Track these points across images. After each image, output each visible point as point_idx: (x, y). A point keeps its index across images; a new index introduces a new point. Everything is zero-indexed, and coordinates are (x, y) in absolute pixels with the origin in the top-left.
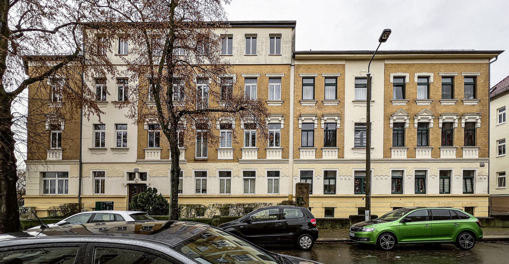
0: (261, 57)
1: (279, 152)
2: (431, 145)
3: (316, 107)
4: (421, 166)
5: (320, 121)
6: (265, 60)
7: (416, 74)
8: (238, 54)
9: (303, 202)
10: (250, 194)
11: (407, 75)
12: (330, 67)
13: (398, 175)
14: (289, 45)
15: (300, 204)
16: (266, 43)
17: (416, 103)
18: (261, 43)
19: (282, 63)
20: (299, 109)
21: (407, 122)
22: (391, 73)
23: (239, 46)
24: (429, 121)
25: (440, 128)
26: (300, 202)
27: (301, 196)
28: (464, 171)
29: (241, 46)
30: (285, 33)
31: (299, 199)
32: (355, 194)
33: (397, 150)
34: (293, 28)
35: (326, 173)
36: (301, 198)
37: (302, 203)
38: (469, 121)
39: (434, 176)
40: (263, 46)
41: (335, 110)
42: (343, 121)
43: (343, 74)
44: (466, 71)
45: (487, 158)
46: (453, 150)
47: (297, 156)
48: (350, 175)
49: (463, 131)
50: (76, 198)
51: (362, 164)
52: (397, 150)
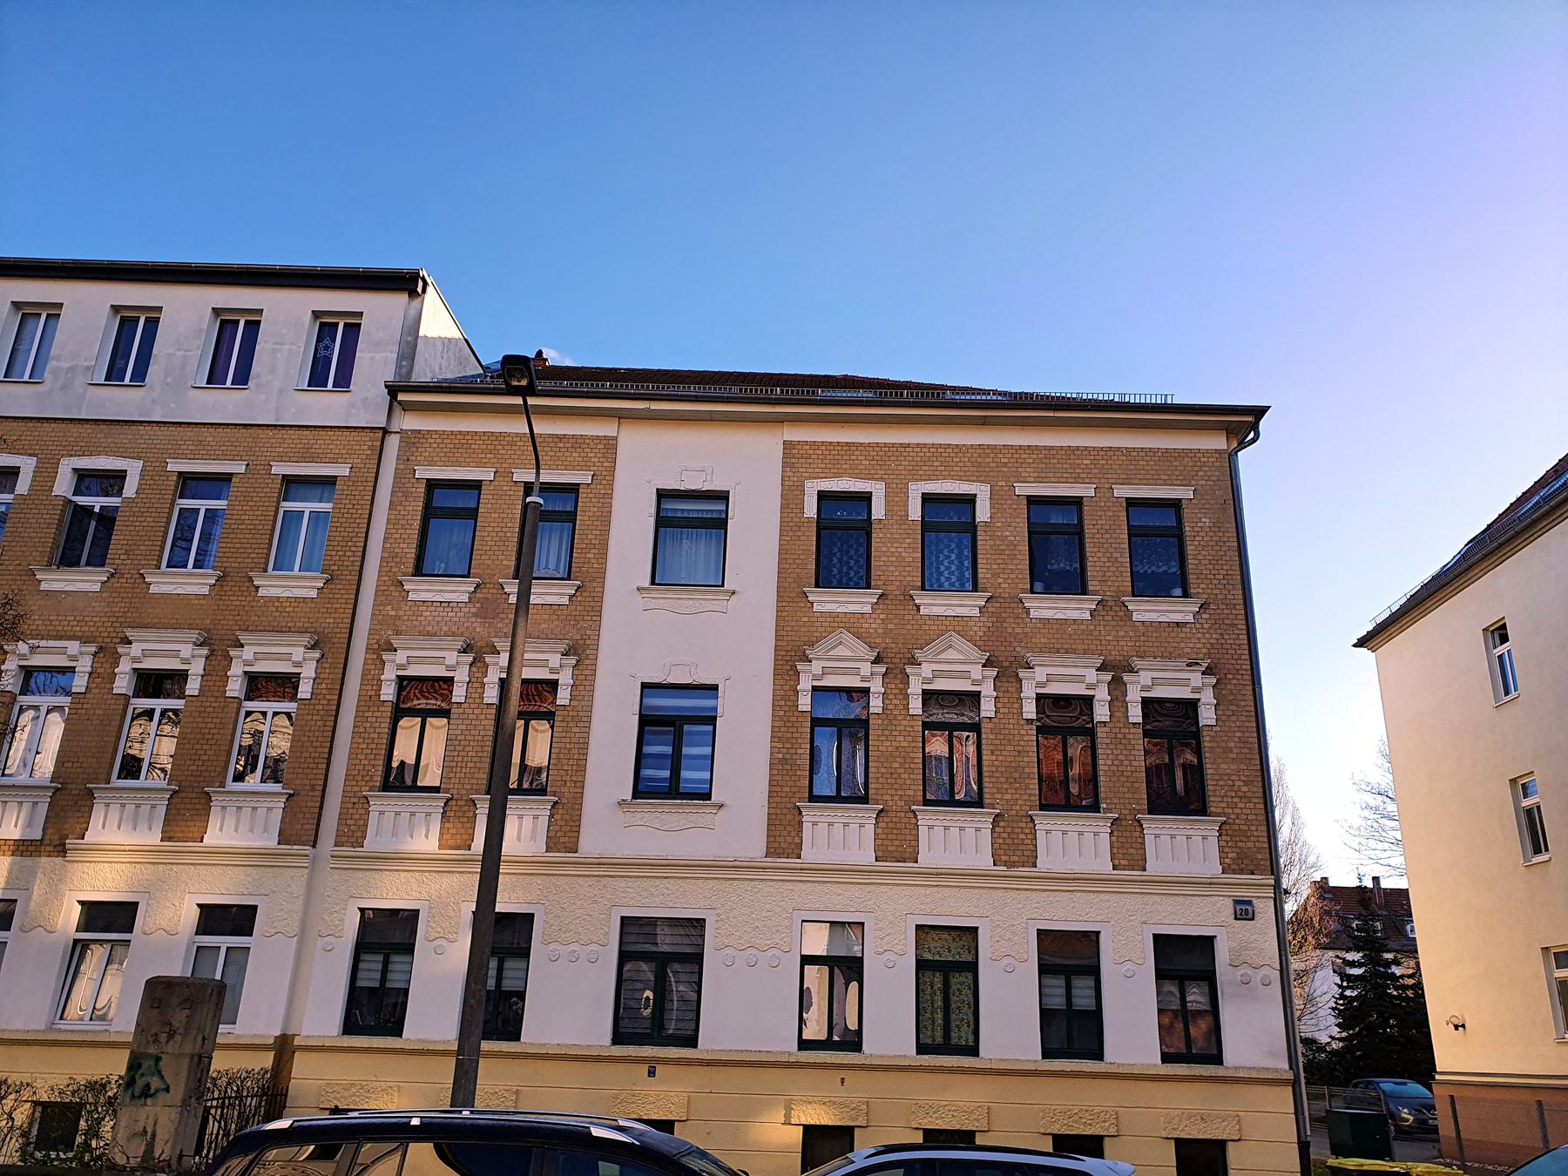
0: (264, 397)
1: (238, 807)
2: (992, 801)
3: (473, 610)
4: (951, 909)
5: (796, 677)
6: (277, 408)
7: (914, 487)
8: (169, 380)
9: (155, 1083)
10: (91, 1028)
11: (878, 490)
12: (552, 445)
13: (950, 952)
14: (389, 354)
15: (138, 1090)
16: (292, 344)
17: (918, 607)
18: (274, 344)
19: (347, 422)
20: (393, 613)
21: (1203, 700)
22: (810, 478)
23: (179, 353)
24: (1196, 696)
25: (1029, 721)
26: (140, 1083)
27: (152, 1050)
28: (1046, 938)
29: (186, 351)
30: (377, 309)
31: (140, 1066)
32: (1164, 1061)
33: (1077, 828)
34: (413, 293)
35: (1165, 945)
36: (151, 1056)
37: (148, 1086)
38: (1159, 692)
39: (1011, 960)
40: (279, 355)
41: (556, 623)
42: (587, 672)
43: (605, 478)
44: (1134, 481)
45: (308, 849)
46: (1191, 832)
47: (350, 833)
48: (595, 939)
49: (1138, 742)
50: (445, 1053)
51: (658, 882)
52: (1077, 828)
